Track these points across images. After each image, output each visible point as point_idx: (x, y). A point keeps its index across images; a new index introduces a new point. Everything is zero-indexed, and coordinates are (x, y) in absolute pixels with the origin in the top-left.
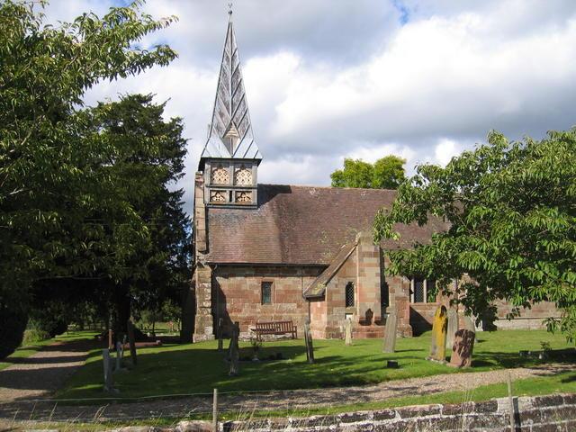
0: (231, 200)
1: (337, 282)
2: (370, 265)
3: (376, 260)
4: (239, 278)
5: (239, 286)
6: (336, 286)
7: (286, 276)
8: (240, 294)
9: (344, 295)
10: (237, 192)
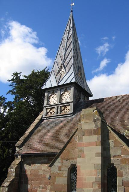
0: (57, 113)
1: (59, 165)
2: (90, 144)
3: (96, 138)
4: (37, 165)
5: (37, 170)
6: (60, 168)
7: (101, 173)
8: (37, 177)
9: (66, 179)
10: (61, 107)
